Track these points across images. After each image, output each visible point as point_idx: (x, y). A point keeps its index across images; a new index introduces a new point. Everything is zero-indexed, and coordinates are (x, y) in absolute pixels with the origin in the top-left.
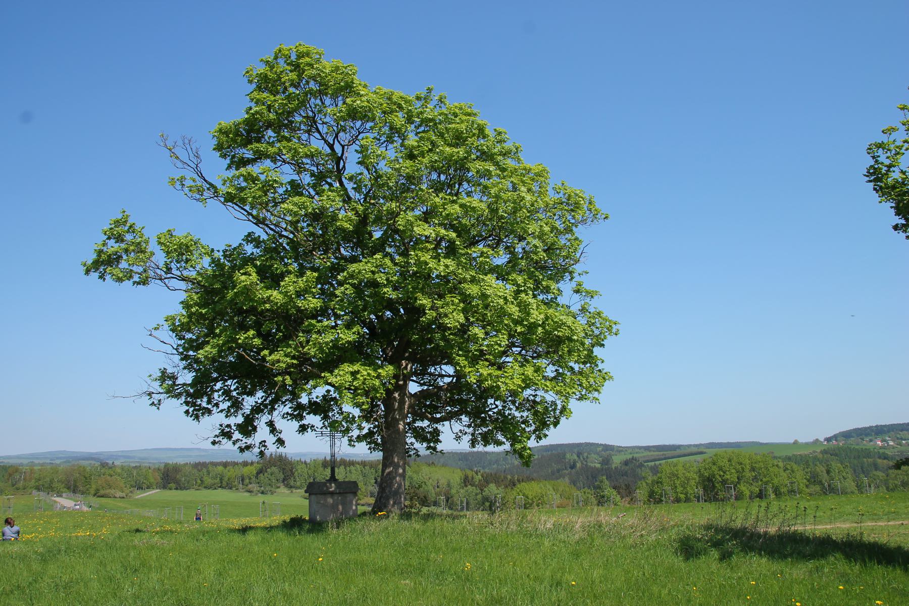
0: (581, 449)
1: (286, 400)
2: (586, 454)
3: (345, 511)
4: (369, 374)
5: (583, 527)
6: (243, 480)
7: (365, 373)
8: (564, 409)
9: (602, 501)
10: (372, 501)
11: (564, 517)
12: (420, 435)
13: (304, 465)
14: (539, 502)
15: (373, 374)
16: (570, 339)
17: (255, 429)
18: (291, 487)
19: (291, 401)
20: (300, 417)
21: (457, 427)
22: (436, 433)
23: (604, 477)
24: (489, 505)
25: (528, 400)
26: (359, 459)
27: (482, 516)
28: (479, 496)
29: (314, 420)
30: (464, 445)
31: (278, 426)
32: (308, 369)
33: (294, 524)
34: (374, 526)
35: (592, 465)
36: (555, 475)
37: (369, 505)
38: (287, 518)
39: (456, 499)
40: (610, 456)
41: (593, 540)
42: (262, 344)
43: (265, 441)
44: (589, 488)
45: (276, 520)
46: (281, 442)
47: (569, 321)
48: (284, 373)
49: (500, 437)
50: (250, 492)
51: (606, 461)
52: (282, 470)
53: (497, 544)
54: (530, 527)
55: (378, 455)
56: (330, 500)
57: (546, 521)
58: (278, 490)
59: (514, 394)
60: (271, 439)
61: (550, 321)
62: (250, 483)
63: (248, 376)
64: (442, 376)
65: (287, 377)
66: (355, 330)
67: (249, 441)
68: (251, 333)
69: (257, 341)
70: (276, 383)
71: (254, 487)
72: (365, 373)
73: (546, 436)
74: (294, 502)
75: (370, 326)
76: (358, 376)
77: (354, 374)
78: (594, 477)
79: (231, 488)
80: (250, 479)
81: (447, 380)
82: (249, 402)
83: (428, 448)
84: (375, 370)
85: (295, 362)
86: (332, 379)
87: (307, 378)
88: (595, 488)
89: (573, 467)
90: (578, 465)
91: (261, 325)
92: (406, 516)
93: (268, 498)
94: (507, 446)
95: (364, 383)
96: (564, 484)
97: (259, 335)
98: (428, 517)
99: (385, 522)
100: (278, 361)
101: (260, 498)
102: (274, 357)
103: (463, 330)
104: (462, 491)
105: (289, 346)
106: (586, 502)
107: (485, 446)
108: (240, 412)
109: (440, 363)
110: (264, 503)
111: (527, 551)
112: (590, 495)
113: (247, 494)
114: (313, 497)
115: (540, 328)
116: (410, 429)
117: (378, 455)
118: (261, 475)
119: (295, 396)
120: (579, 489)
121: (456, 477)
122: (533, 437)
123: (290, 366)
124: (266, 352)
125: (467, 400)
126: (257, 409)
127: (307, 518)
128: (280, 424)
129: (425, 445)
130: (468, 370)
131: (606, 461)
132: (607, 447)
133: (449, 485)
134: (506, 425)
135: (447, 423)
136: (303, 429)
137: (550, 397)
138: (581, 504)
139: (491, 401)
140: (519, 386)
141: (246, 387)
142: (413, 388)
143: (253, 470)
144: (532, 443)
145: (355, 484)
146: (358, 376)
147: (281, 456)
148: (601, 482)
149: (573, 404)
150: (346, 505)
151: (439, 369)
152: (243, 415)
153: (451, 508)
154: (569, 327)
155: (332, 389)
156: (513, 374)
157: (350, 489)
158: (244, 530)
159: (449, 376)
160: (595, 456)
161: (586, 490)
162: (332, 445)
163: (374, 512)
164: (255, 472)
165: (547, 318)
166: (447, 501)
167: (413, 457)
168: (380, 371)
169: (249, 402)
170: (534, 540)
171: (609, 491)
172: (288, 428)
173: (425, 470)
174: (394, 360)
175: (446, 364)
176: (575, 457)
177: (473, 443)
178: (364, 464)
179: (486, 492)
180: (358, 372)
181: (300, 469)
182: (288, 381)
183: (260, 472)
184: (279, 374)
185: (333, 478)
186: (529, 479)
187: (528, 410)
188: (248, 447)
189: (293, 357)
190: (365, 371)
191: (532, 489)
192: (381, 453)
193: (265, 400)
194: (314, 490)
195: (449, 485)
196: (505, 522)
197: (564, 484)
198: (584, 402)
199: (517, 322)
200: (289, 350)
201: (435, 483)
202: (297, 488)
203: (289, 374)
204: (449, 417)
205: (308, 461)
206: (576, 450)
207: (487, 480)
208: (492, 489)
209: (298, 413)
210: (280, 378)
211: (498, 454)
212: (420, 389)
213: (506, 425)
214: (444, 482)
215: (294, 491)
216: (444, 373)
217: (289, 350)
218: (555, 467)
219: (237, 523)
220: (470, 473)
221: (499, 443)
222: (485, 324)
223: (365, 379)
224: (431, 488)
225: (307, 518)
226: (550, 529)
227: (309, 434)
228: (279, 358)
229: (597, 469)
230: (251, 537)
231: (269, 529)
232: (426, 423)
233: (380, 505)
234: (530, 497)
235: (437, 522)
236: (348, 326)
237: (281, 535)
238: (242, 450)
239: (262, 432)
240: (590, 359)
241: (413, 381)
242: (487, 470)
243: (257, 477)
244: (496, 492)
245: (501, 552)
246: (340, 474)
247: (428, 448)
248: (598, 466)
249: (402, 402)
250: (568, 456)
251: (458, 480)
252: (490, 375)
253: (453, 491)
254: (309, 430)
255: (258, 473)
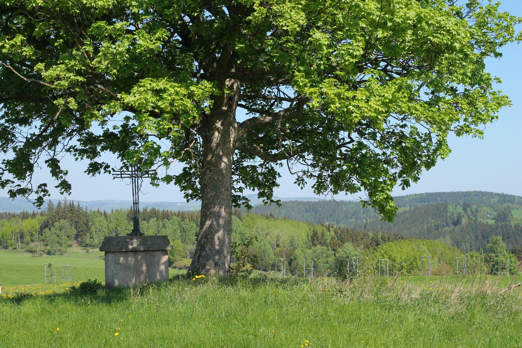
0: (469, 200)
1: (73, 131)
2: (475, 207)
3: (150, 274)
4: (177, 93)
5: (461, 299)
6: (22, 237)
7: (172, 91)
8: (440, 144)
9: (495, 269)
10: (188, 262)
11: (434, 286)
12: (250, 178)
13: (103, 217)
14: (411, 268)
15: (183, 91)
16: (450, 49)
17: (30, 168)
18: (87, 245)
19: (79, 131)
20: (94, 153)
21: (298, 166)
22: (272, 174)
23: (500, 238)
24: (341, 270)
25: (393, 133)
26: (175, 210)
27: (330, 282)
28: (331, 259)
29: (109, 157)
30: (308, 193)
31: (63, 166)
32: (96, 90)
33: (88, 290)
34: (190, 292)
35: (484, 221)
36: (432, 233)
37: (185, 267)
38: (77, 285)
39: (302, 262)
40: (509, 209)
41: (473, 316)
42: (35, 53)
43: (45, 185)
44: (478, 250)
45: (65, 286)
46: (66, 186)
47: (450, 23)
48: (69, 93)
49: (355, 181)
50: (32, 252)
51: (503, 217)
52: (77, 222)
53: (346, 317)
54: (390, 296)
55: (196, 205)
56: (131, 260)
57: (411, 288)
58: (69, 249)
59: (372, 122)
60: (52, 182)
61: (424, 24)
62: (32, 241)
63: (20, 97)
64: (281, 100)
65: (71, 99)
66: (158, 35)
67: (24, 185)
68: (19, 39)
69: (28, 51)
70: (55, 108)
71: (37, 245)
72: (172, 91)
73: (416, 179)
74: (89, 264)
75: (183, 31)
76: (165, 96)
77: (158, 92)
78: (486, 237)
79: (6, 248)
80: (32, 235)
81: (286, 105)
82: (23, 133)
83: (261, 195)
84: (187, 88)
85: (81, 79)
86: (129, 99)
87: (98, 101)
88: (485, 251)
89: (457, 223)
90: (464, 221)
91: (33, 27)
92: (229, 279)
93: (56, 260)
94: (363, 195)
95: (171, 104)
96: (443, 244)
97: (30, 40)
98: (256, 282)
99: (201, 289)
100: (58, 78)
101: (46, 259)
102: (52, 72)
103: (303, 34)
104: (309, 251)
105: (72, 57)
106: (472, 269)
107: (335, 192)
108: (11, 145)
109: (277, 84)
110: (50, 265)
111: (385, 327)
112: (478, 257)
113: (29, 255)
114: (110, 256)
115: (410, 32)
116: (237, 169)
117: (196, 205)
118: (47, 230)
119: (83, 125)
120: (464, 252)
121: (301, 233)
122: (399, 181)
123: (74, 84)
124: (40, 66)
125: (312, 133)
126: (33, 143)
127: (103, 283)
128: (66, 161)
129: (257, 192)
130: (307, 90)
131: (503, 217)
132: (504, 198)
133: (292, 243)
134: (365, 167)
135: (284, 162)
136: (94, 168)
137: (423, 129)
138: (465, 271)
139: (343, 134)
140: (376, 111)
141: (18, 113)
142: (242, 115)
143: (36, 223)
144: (397, 191)
145: (165, 240)
146: (165, 96)
147: (72, 206)
148: (495, 243)
149: (451, 137)
150: (152, 266)
151: (275, 91)
152: (14, 149)
153: (292, 272)
154: (448, 31)
155: (131, 114)
156: (371, 95)
157: (158, 245)
158: (19, 299)
159: (289, 100)
160: (489, 210)
161: (474, 253)
162: (136, 190)
163: (189, 276)
164: (38, 227)
165: (420, 19)
166: (290, 264)
167: (242, 206)
168: (192, 88)
169: (23, 133)
170: (394, 313)
171: (504, 257)
172: (74, 166)
173: (262, 223)
174: (215, 75)
175: (283, 83)
176: (460, 210)
177: (320, 187)
178: (182, 216)
179: (341, 253)
180: (165, 90)
181: (98, 223)
182: (73, 104)
183: (45, 226)
184: (61, 96)
185: (136, 232)
186: (398, 237)
187: (394, 147)
188: (23, 191)
189: (79, 73)
190: (172, 89)
191: (402, 250)
192: (200, 202)
193: (45, 130)
194: (111, 246)
195: (292, 243)
196: (362, 288)
197: (443, 244)
198: (465, 137)
199: (376, 25)
200: (73, 63)
201: (274, 241)
202: (94, 247)
203: (74, 95)
204: (286, 155)
205: (109, 212)
206: (461, 201)
207: (342, 238)
208: (349, 249)
209: (90, 146)
210: (61, 101)
211: (356, 204)
212: (251, 116)
213: (365, 167)
214: (285, 239)
215: (91, 250)
216: (282, 96)
217: (73, 63)
218: (433, 222)
219: (12, 291)
220: (320, 229)
221: (352, 189)
222: (335, 29)
223: (174, 100)
224: (269, 246)
225: (103, 283)
226: (416, 299)
227: (102, 176)
228: (59, 74)
229: (490, 226)
230: (27, 307)
231: (51, 298)
232: (258, 161)
233: (196, 269)
234: (398, 261)
235: (268, 289)
236: (151, 29)
237: (68, 306)
238: (13, 194)
239: (41, 173)
240: (478, 78)
241: (241, 106)
242: (342, 225)
243: (41, 232)
244: (353, 253)
245: (350, 327)
246: (149, 228)
247: (261, 195)
248: (491, 222)
249: (225, 135)
250: (450, 208)
251: (305, 237)
252: (338, 95)
253: (298, 252)
254: (102, 170)
255: (42, 228)
